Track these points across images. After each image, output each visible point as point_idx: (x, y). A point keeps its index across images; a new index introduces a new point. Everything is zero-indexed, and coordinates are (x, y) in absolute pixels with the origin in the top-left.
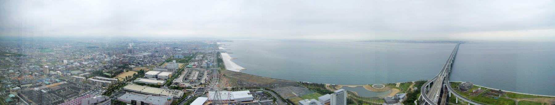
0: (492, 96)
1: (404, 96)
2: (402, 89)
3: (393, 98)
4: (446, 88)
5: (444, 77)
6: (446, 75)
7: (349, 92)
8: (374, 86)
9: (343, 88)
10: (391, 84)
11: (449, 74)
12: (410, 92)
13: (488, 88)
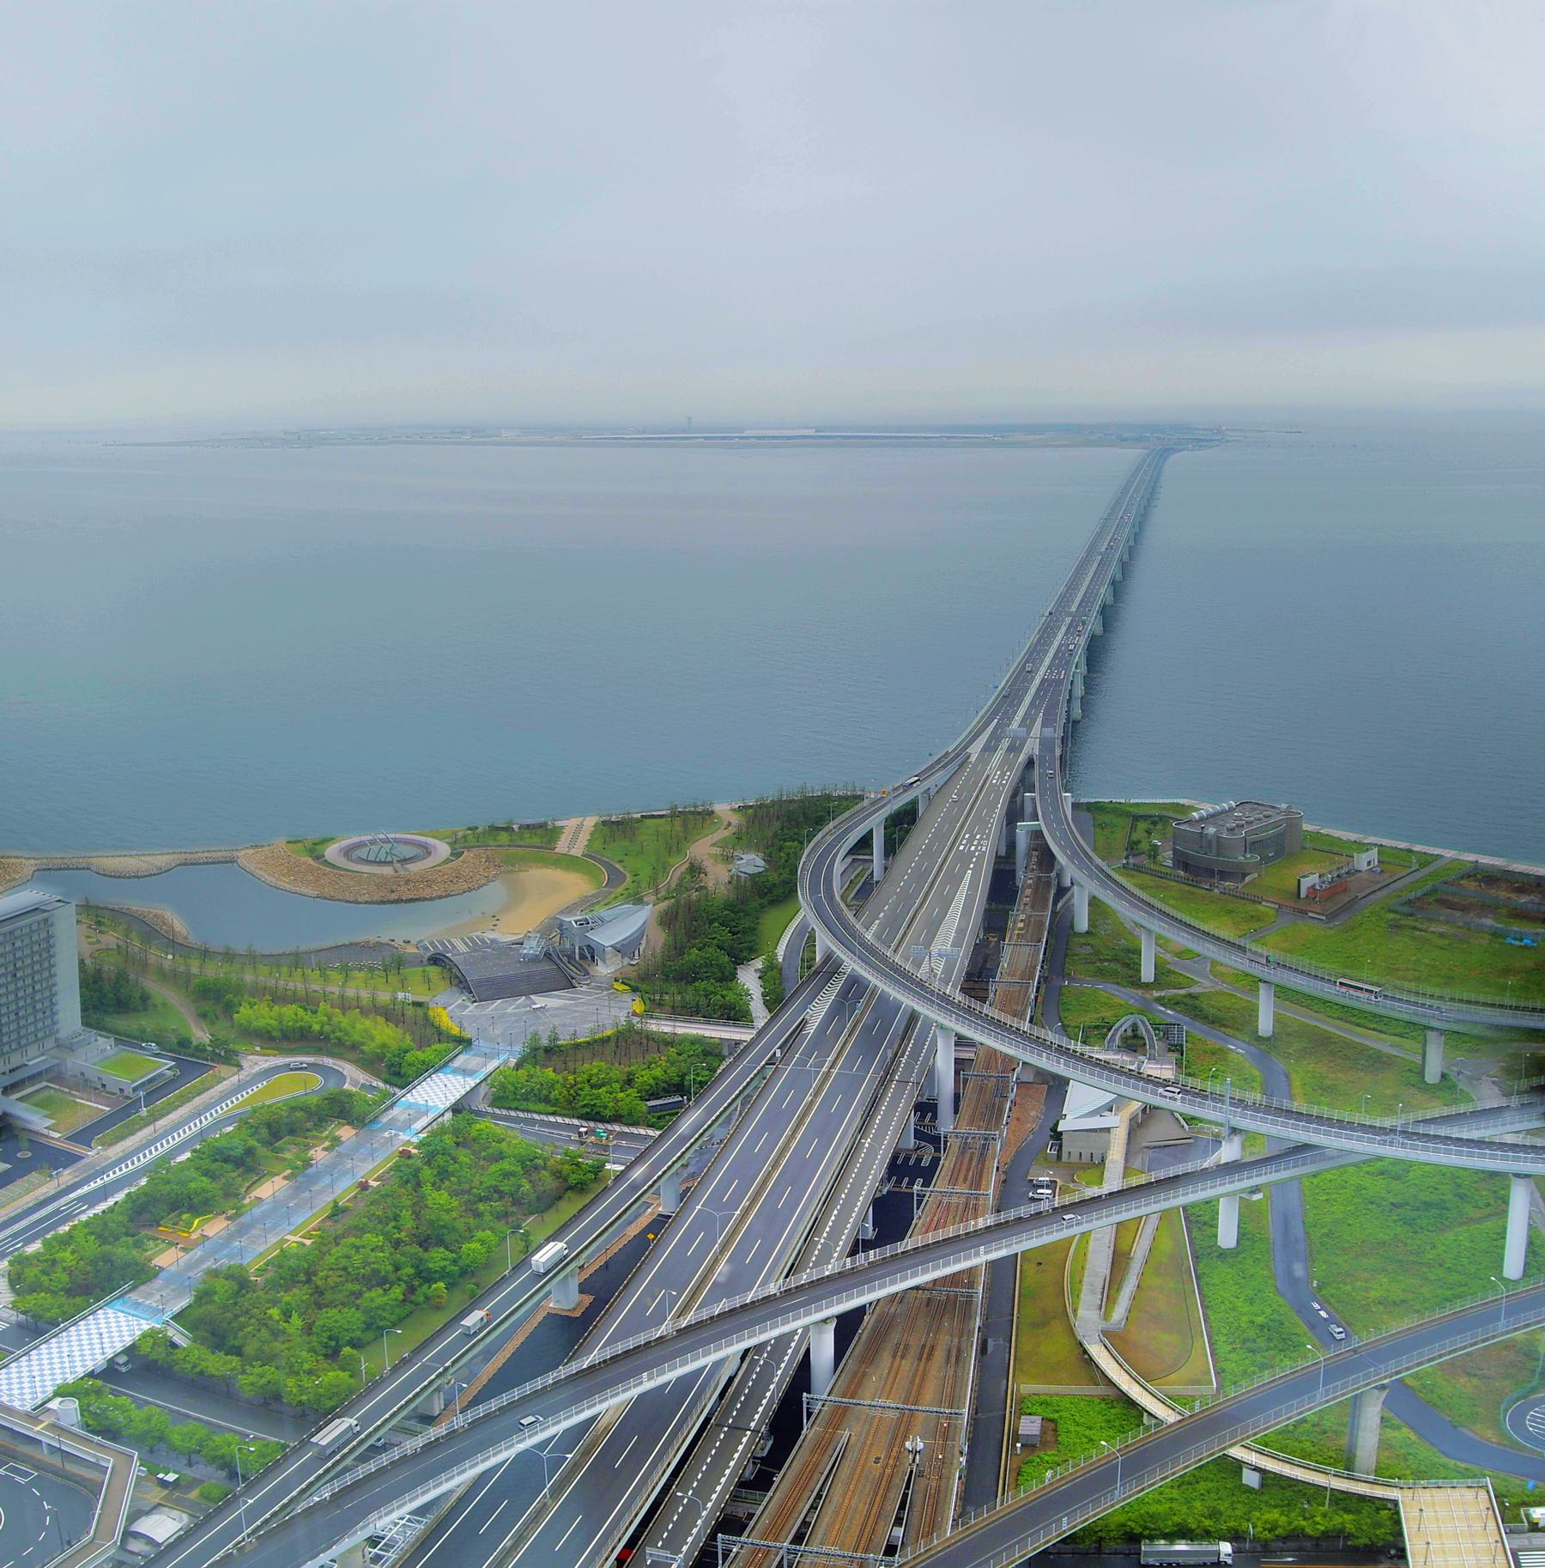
0: (1488, 922)
1: (641, 933)
2: (611, 869)
3: (532, 948)
4: (1046, 859)
5: (1022, 758)
6: (1045, 744)
7: (95, 915)
8: (347, 852)
9: (46, 873)
10: (508, 829)
11: (1073, 731)
12: (694, 895)
13: (1449, 854)
